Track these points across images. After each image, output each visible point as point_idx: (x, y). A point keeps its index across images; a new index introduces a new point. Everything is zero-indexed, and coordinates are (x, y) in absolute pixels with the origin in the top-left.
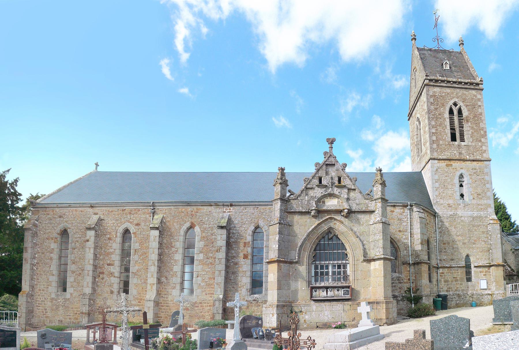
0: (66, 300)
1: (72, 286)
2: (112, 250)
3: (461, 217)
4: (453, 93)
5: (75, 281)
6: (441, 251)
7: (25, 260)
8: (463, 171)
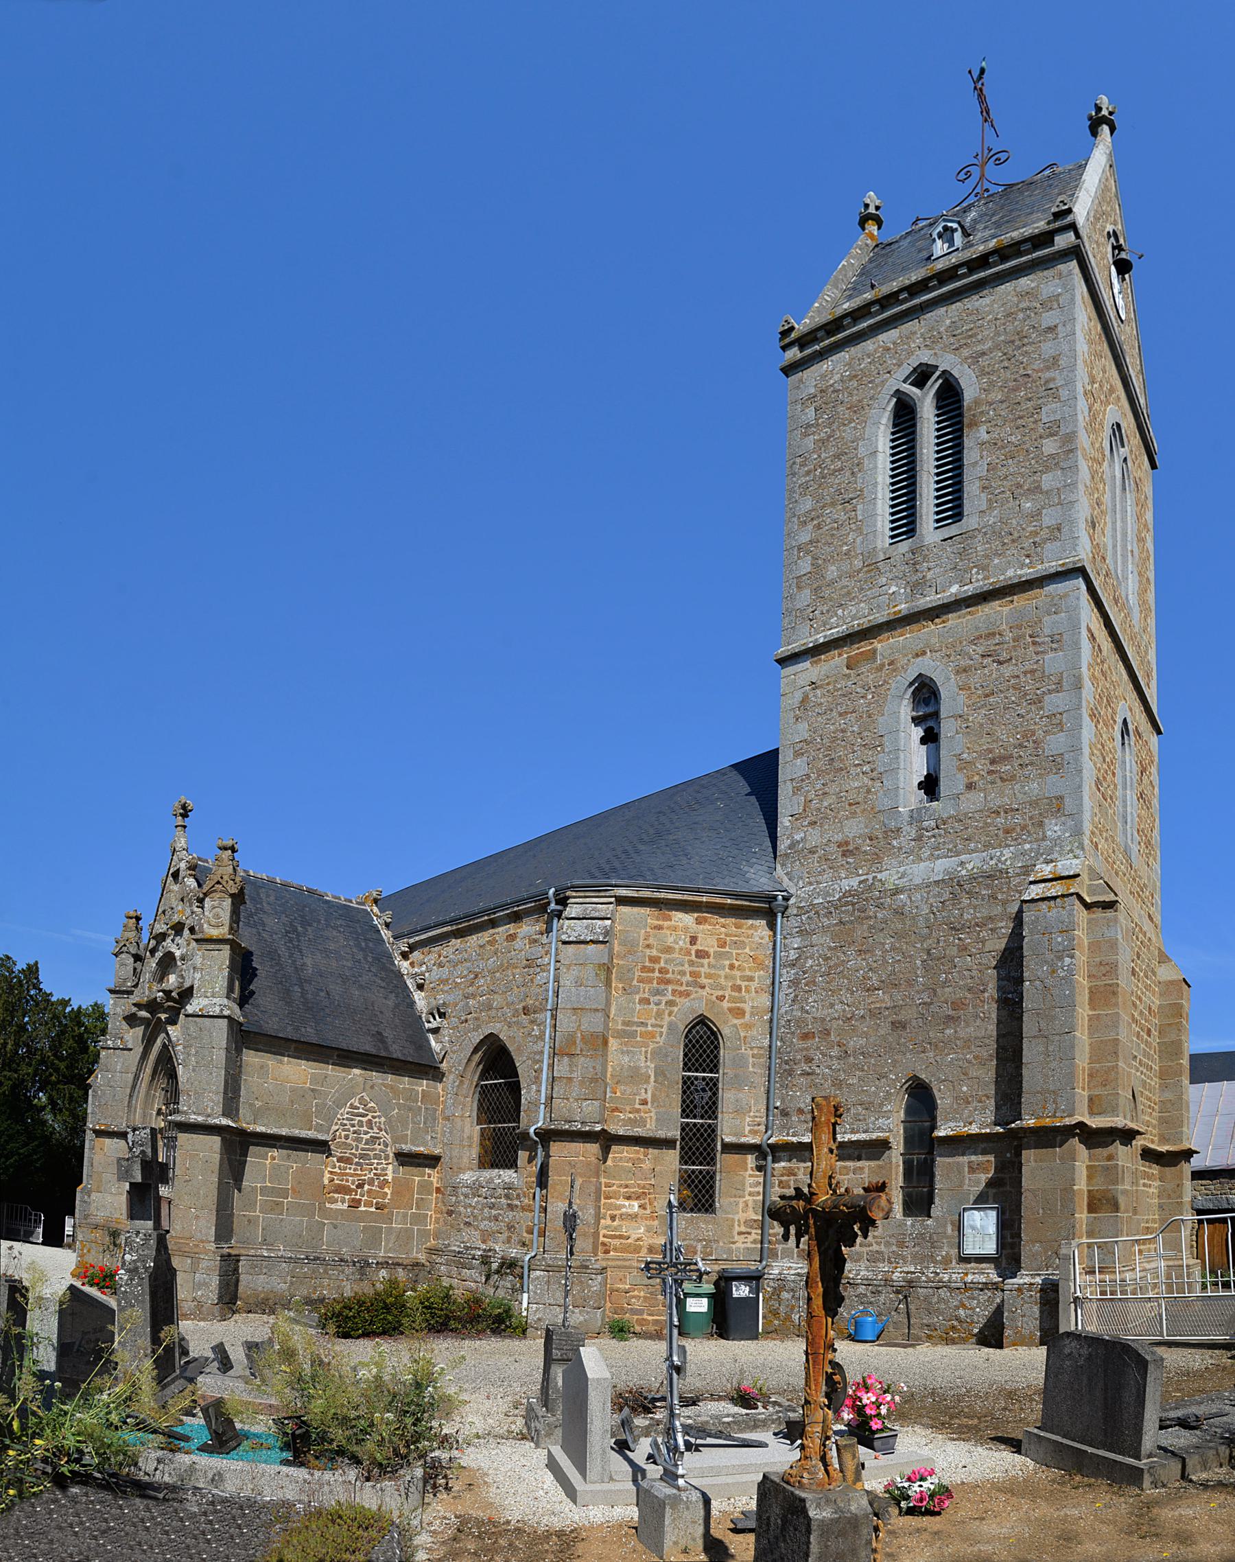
3: (897, 891)
6: (790, 1073)
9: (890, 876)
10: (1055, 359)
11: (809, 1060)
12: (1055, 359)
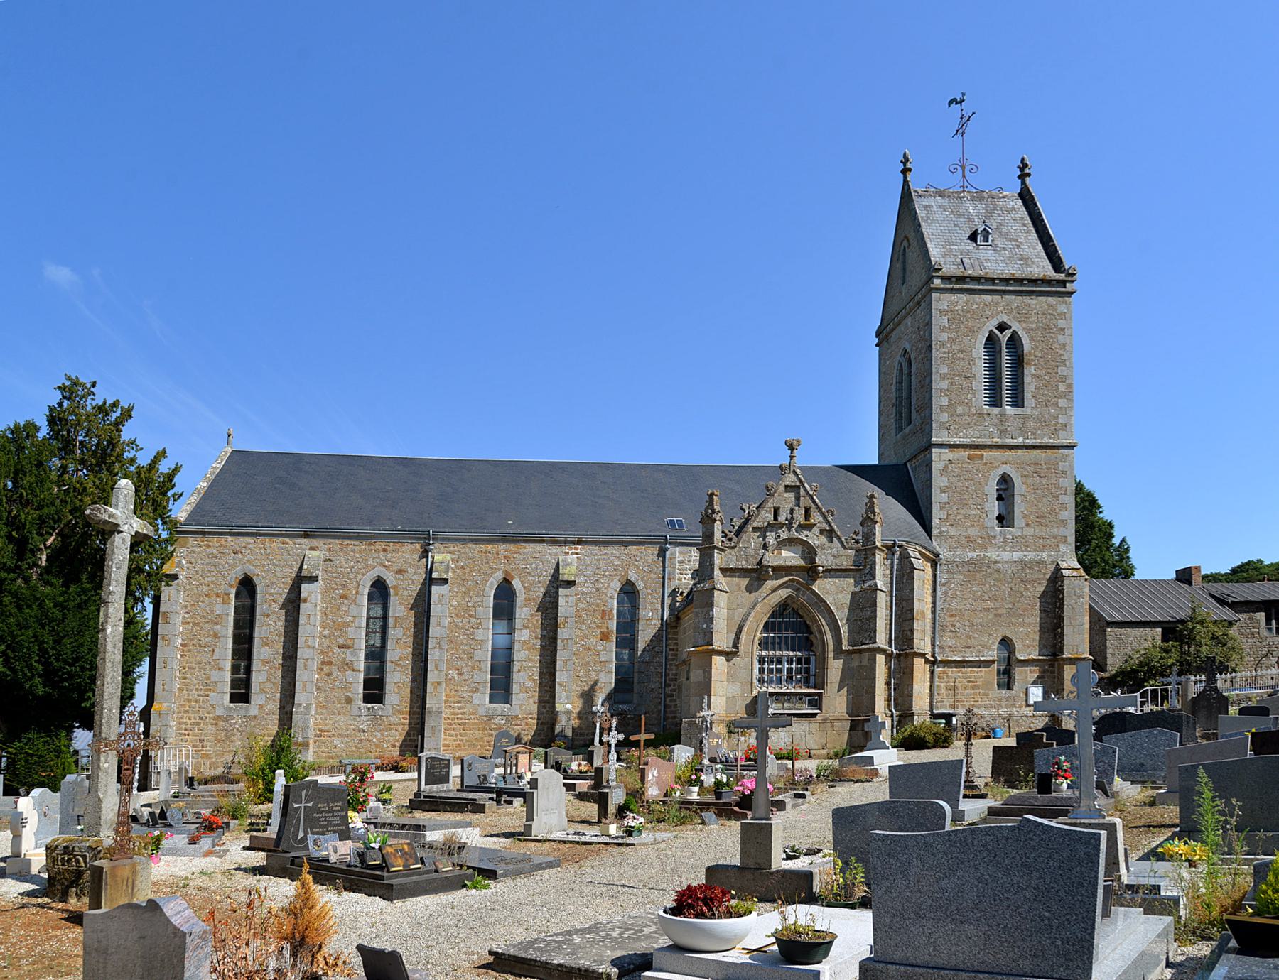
0: (249, 719)
1: (263, 691)
3: (997, 562)
4: (998, 303)
5: (269, 680)
8: (1007, 469)
9: (992, 554)
10: (1064, 345)
11: (953, 626)
12: (1064, 345)
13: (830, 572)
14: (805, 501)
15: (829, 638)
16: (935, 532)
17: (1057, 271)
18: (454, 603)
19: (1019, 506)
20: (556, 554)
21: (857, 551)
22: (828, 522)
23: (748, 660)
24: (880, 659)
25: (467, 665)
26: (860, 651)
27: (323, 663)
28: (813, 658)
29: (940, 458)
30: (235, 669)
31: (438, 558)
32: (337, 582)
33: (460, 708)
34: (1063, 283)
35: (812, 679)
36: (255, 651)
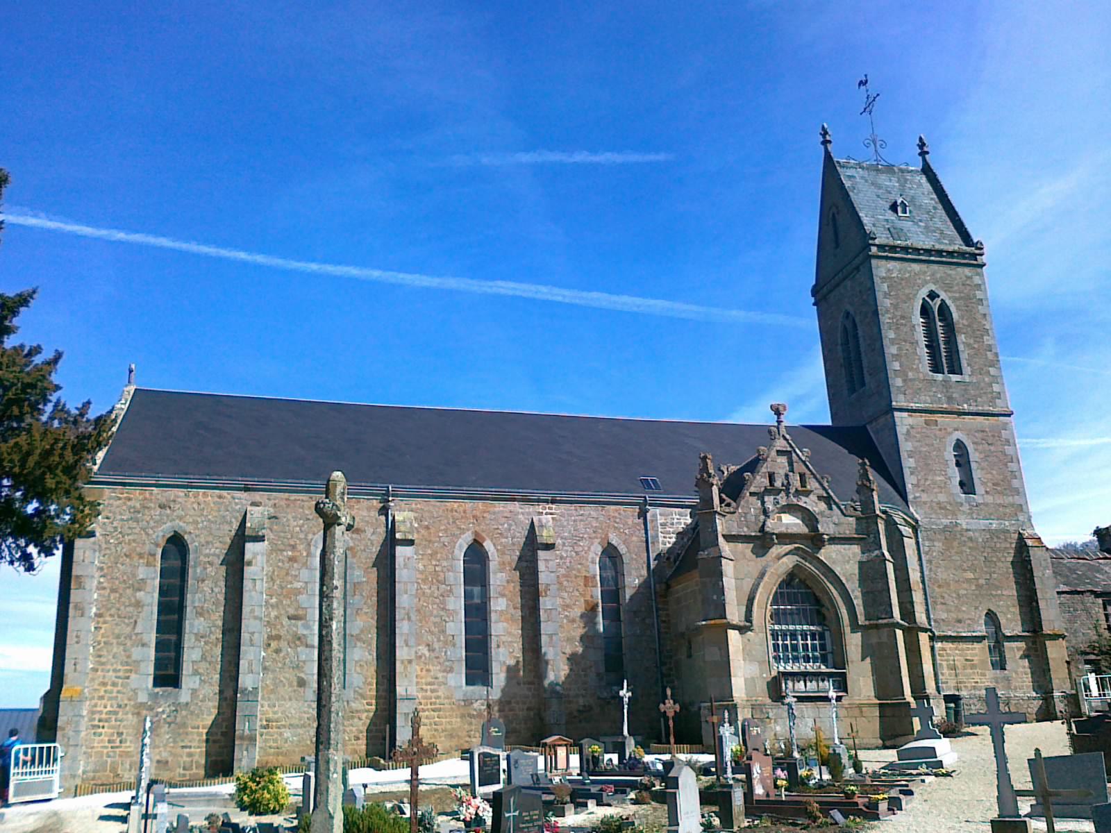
1: (196, 672)
2: (298, 585)
3: (968, 530)
4: (925, 272)
5: (203, 658)
7: (76, 607)
10: (985, 315)
11: (943, 597)
12: (985, 315)
13: (834, 540)
14: (799, 467)
15: (844, 611)
16: (910, 497)
17: (968, 245)
18: (421, 566)
19: (977, 475)
20: (529, 514)
21: (858, 519)
22: (824, 489)
23: (762, 635)
24: (899, 633)
25: (439, 640)
26: (877, 627)
27: (270, 637)
28: (827, 634)
29: (903, 421)
30: (160, 646)
31: (399, 517)
32: (285, 542)
33: (432, 691)
34: (974, 256)
35: (830, 657)
36: (187, 624)
